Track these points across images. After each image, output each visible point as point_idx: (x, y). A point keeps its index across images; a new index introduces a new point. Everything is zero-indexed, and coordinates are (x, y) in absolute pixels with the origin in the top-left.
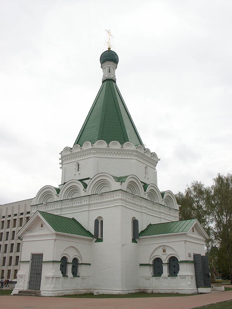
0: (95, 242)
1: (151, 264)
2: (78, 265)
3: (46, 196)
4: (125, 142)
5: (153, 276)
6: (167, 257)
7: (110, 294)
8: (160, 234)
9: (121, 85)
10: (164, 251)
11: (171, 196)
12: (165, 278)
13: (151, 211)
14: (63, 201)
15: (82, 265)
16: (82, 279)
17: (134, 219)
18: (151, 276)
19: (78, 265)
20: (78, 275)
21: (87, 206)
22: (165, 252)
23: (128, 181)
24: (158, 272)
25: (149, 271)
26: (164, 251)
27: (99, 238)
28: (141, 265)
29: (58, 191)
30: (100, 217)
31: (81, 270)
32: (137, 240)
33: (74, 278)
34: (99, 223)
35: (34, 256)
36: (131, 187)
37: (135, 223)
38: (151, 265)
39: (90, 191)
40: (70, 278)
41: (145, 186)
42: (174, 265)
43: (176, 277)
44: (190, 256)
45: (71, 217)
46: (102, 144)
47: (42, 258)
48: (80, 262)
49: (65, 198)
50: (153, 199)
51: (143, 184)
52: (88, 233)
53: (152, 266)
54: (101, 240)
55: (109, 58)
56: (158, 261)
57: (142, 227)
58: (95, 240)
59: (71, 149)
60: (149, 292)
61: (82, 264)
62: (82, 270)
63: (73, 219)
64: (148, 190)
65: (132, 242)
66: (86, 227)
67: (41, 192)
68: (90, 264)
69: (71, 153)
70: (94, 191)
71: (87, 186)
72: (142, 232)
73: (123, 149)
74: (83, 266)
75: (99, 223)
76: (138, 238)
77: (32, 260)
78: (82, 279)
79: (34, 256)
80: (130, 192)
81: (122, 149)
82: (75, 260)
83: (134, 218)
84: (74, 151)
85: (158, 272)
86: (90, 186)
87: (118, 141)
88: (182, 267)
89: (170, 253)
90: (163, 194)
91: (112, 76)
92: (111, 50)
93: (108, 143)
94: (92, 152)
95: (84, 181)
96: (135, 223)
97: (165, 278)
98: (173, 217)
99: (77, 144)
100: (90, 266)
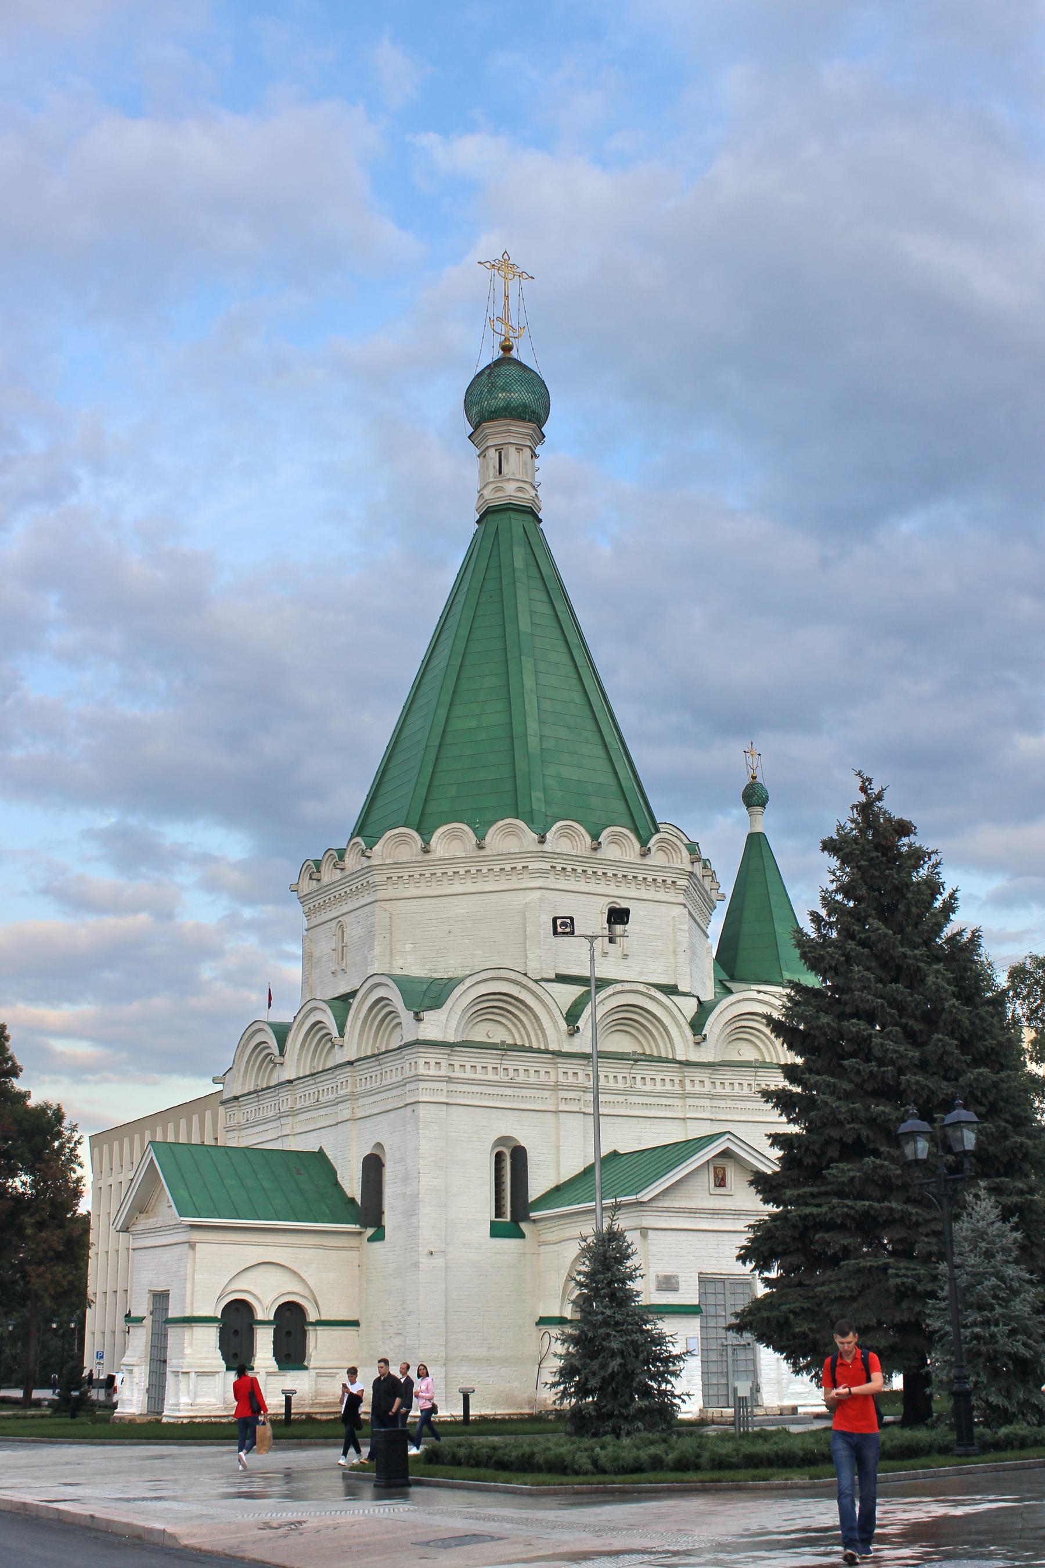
8: (512, 1206)
13: (621, 1098)
14: (295, 1083)
15: (318, 1328)
16: (318, 1375)
20: (306, 1363)
21: (290, 1120)
23: (460, 1000)
28: (355, 1323)
29: (282, 1032)
31: (316, 1348)
32: (523, 1226)
33: (283, 1373)
34: (373, 1167)
36: (502, 1015)
37: (512, 1163)
39: (355, 1047)
47: (167, 1309)
49: (262, 1081)
50: (649, 1043)
55: (506, 401)
68: (355, 1323)
69: (419, 858)
70: (367, 1044)
73: (482, 853)
78: (318, 1375)
86: (353, 1027)
92: (514, 354)
94: (531, 866)
96: (512, 1163)
99: (358, 835)
100: (356, 1328)
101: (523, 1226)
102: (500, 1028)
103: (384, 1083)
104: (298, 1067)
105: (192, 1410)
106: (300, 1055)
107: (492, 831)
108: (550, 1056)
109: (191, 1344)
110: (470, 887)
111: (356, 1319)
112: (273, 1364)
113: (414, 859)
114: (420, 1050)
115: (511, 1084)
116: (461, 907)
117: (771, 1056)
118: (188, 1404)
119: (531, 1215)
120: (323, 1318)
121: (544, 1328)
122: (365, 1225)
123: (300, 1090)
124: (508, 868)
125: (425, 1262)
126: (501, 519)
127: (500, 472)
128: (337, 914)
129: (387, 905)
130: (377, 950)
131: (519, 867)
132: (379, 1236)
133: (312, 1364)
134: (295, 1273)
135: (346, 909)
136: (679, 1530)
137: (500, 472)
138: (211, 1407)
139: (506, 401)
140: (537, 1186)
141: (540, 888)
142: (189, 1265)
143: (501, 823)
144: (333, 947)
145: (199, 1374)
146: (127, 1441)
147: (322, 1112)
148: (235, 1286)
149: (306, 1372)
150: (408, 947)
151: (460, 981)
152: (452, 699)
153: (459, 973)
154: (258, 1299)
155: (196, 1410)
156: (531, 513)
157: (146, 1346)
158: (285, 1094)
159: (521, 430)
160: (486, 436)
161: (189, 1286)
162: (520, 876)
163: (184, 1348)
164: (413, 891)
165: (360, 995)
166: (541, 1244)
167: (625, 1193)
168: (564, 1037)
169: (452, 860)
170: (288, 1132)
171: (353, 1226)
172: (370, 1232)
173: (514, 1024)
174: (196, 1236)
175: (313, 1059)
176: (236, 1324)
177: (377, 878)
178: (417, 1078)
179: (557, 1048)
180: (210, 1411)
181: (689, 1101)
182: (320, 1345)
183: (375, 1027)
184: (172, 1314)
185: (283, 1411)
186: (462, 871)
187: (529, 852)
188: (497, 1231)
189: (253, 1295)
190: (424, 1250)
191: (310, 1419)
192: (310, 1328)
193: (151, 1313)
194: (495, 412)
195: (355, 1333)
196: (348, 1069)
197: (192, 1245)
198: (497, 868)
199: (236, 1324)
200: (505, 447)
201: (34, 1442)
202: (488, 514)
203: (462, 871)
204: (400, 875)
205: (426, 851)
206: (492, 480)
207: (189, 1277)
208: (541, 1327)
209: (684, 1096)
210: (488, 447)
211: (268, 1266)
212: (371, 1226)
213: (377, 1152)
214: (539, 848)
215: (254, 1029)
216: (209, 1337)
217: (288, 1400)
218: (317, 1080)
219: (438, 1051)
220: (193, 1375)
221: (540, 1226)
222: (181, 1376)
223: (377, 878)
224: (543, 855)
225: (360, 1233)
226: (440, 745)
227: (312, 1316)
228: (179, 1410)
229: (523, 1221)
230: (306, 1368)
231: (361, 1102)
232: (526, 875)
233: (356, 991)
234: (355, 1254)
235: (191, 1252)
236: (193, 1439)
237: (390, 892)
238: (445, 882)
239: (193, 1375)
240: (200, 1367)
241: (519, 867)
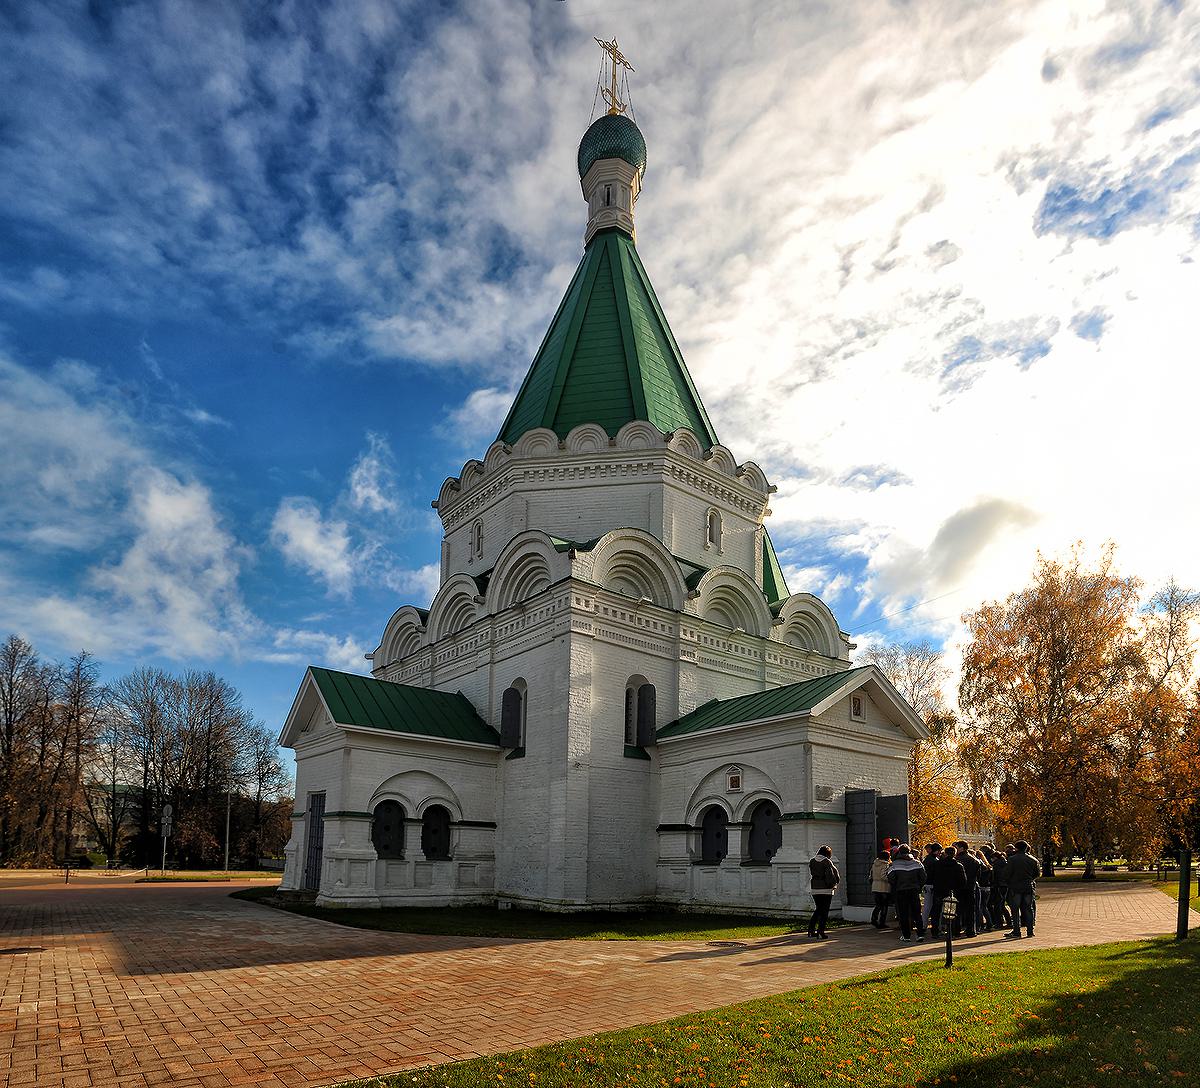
0: (507, 758)
1: (692, 823)
2: (405, 823)
3: (407, 639)
7: (371, 909)
9: (661, 258)
10: (735, 782)
11: (814, 612)
19: (405, 823)
24: (712, 852)
25: (679, 846)
26: (735, 782)
29: (424, 616)
30: (635, 678)
34: (514, 699)
38: (695, 828)
40: (412, 862)
42: (765, 824)
43: (768, 869)
52: (486, 733)
54: (519, 753)
56: (718, 816)
60: (683, 909)
62: (463, 841)
65: (625, 756)
66: (484, 716)
67: (391, 629)
68: (492, 825)
69: (555, 454)
75: (514, 699)
76: (658, 747)
77: (310, 810)
78: (461, 866)
85: (712, 852)
86: (494, 586)
88: (789, 832)
96: (640, 698)
97: (730, 870)
103: (526, 626)
110: (598, 480)
132: (519, 753)
134: (442, 781)
136: (80, 852)
140: (662, 718)
148: (387, 789)
152: (568, 374)
154: (408, 801)
162: (645, 472)
165: (495, 572)
167: (757, 715)
172: (508, 752)
176: (387, 823)
187: (534, 630)
188: (925, 253)
189: (400, 795)
197: (348, 751)
199: (387, 823)
205: (562, 448)
211: (418, 774)
213: (517, 687)
215: (404, 611)
226: (565, 386)
227: (457, 817)
230: (450, 859)
233: (493, 569)
238: (577, 477)
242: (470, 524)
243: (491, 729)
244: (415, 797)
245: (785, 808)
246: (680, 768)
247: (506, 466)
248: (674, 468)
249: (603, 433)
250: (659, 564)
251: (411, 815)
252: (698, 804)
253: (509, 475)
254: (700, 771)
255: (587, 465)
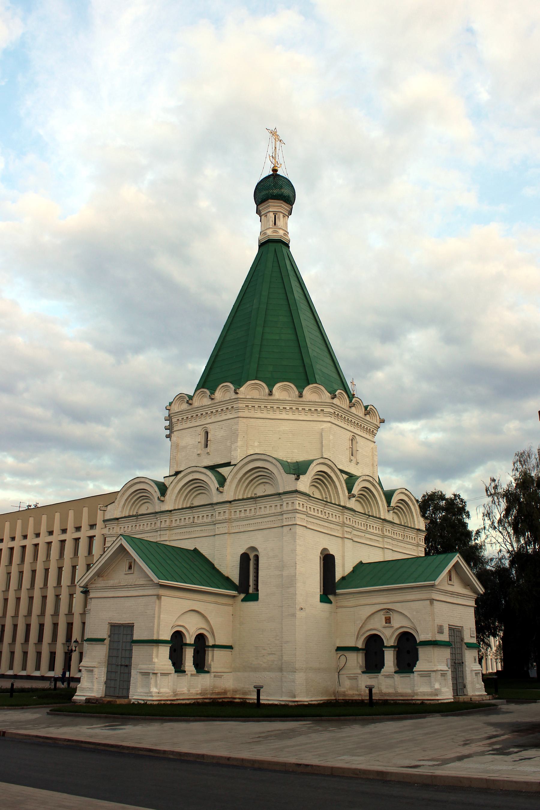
2: (206, 649)
4: (256, 379)
5: (363, 672)
6: (393, 633)
10: (388, 620)
12: (388, 676)
13: (363, 534)
14: (172, 512)
15: (215, 649)
17: (326, 553)
18: (359, 671)
19: (206, 649)
21: (168, 532)
22: (390, 623)
25: (356, 661)
26: (388, 620)
27: (251, 590)
29: (163, 488)
30: (253, 549)
32: (331, 597)
34: (248, 561)
35: (115, 628)
37: (328, 561)
41: (351, 480)
43: (412, 675)
44: (440, 631)
45: (189, 545)
46: (256, 389)
48: (211, 642)
49: (133, 511)
51: (345, 477)
53: (361, 651)
54: (254, 597)
55: (274, 192)
57: (341, 570)
58: (242, 596)
59: (191, 398)
61: (214, 646)
63: (196, 550)
64: (355, 491)
68: (230, 647)
71: (224, 479)
72: (343, 578)
73: (301, 399)
74: (218, 653)
75: (248, 561)
76: (335, 594)
78: (215, 676)
79: (115, 628)
80: (358, 507)
81: (213, 402)
82: (201, 638)
83: (325, 550)
84: (196, 403)
85: (373, 662)
87: (267, 385)
88: (422, 652)
89: (399, 623)
90: (389, 495)
91: (281, 232)
92: (278, 173)
93: (301, 388)
94: (325, 410)
95: (220, 470)
96: (328, 561)
97: (388, 676)
98: (411, 547)
101: (331, 597)
102: (317, 491)
104: (175, 503)
105: (159, 696)
106: (177, 497)
107: (307, 389)
108: (341, 508)
109: (157, 656)
110: (291, 416)
111: (230, 645)
112: (193, 669)
113: (263, 398)
114: (298, 496)
115: (327, 521)
116: (285, 426)
117: (411, 524)
118: (156, 693)
119: (337, 591)
120: (217, 644)
121: (340, 653)
122: (240, 593)
123: (176, 516)
124: (313, 409)
125: (299, 614)
126: (272, 246)
127: (275, 224)
128: (203, 423)
129: (245, 420)
130: (239, 443)
131: (319, 409)
132: (254, 597)
133: (213, 670)
135: (210, 421)
137: (275, 224)
138: (167, 695)
139: (274, 192)
141: (329, 422)
142: (157, 609)
143: (249, 382)
144: (199, 441)
145: (163, 674)
146: (192, 718)
147: (196, 529)
149: (207, 675)
150: (256, 444)
151: (311, 462)
153: (311, 458)
155: (161, 696)
156: (287, 245)
157: (106, 656)
158: (164, 517)
159: (285, 206)
160: (269, 206)
161: (156, 621)
162: (319, 415)
163: (153, 658)
164: (259, 415)
166: (337, 607)
168: (347, 499)
169: (283, 401)
170: (167, 539)
171: (234, 592)
172: (242, 596)
173: (324, 490)
174: (162, 592)
175: (131, 508)
177: (241, 405)
178: (295, 511)
179: (343, 505)
180: (167, 697)
181: (386, 540)
182: (216, 660)
183: (247, 481)
184: (135, 638)
185: (368, 698)
186: (288, 408)
187: (326, 403)
190: (298, 607)
191: (385, 703)
192: (210, 649)
193: (109, 636)
194: (275, 196)
195: (230, 653)
196: (277, 498)
197: (159, 597)
198: (307, 409)
200: (278, 213)
201: (145, 719)
202: (262, 245)
203: (288, 408)
204: (253, 405)
206: (271, 227)
207: (156, 616)
208: (338, 652)
209: (384, 537)
210: (269, 212)
212: (243, 593)
214: (331, 401)
216: (164, 651)
217: (370, 690)
218: (194, 511)
219: (304, 498)
220: (159, 674)
221: (338, 598)
222: (151, 676)
223: (241, 405)
224: (332, 405)
225: (234, 597)
227: (211, 642)
228: (152, 696)
229: (331, 594)
230: (208, 672)
231: (234, 524)
232: (321, 415)
234: (230, 608)
235: (157, 601)
236: (237, 717)
237: (246, 413)
239: (159, 674)
240: (162, 670)
241: (319, 409)
242: (199, 429)
243: (227, 579)
244: (191, 629)
245: (421, 637)
246: (352, 609)
247: (233, 400)
248: (335, 412)
249: (295, 388)
250: (332, 475)
251: (188, 641)
252: (364, 634)
253: (235, 406)
254: (368, 611)
255: (285, 407)
